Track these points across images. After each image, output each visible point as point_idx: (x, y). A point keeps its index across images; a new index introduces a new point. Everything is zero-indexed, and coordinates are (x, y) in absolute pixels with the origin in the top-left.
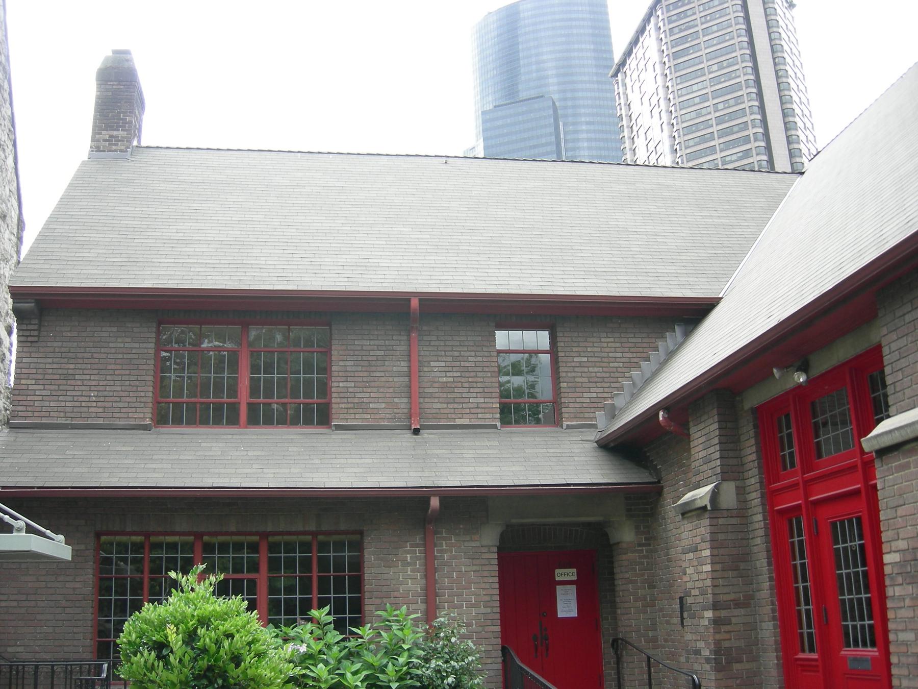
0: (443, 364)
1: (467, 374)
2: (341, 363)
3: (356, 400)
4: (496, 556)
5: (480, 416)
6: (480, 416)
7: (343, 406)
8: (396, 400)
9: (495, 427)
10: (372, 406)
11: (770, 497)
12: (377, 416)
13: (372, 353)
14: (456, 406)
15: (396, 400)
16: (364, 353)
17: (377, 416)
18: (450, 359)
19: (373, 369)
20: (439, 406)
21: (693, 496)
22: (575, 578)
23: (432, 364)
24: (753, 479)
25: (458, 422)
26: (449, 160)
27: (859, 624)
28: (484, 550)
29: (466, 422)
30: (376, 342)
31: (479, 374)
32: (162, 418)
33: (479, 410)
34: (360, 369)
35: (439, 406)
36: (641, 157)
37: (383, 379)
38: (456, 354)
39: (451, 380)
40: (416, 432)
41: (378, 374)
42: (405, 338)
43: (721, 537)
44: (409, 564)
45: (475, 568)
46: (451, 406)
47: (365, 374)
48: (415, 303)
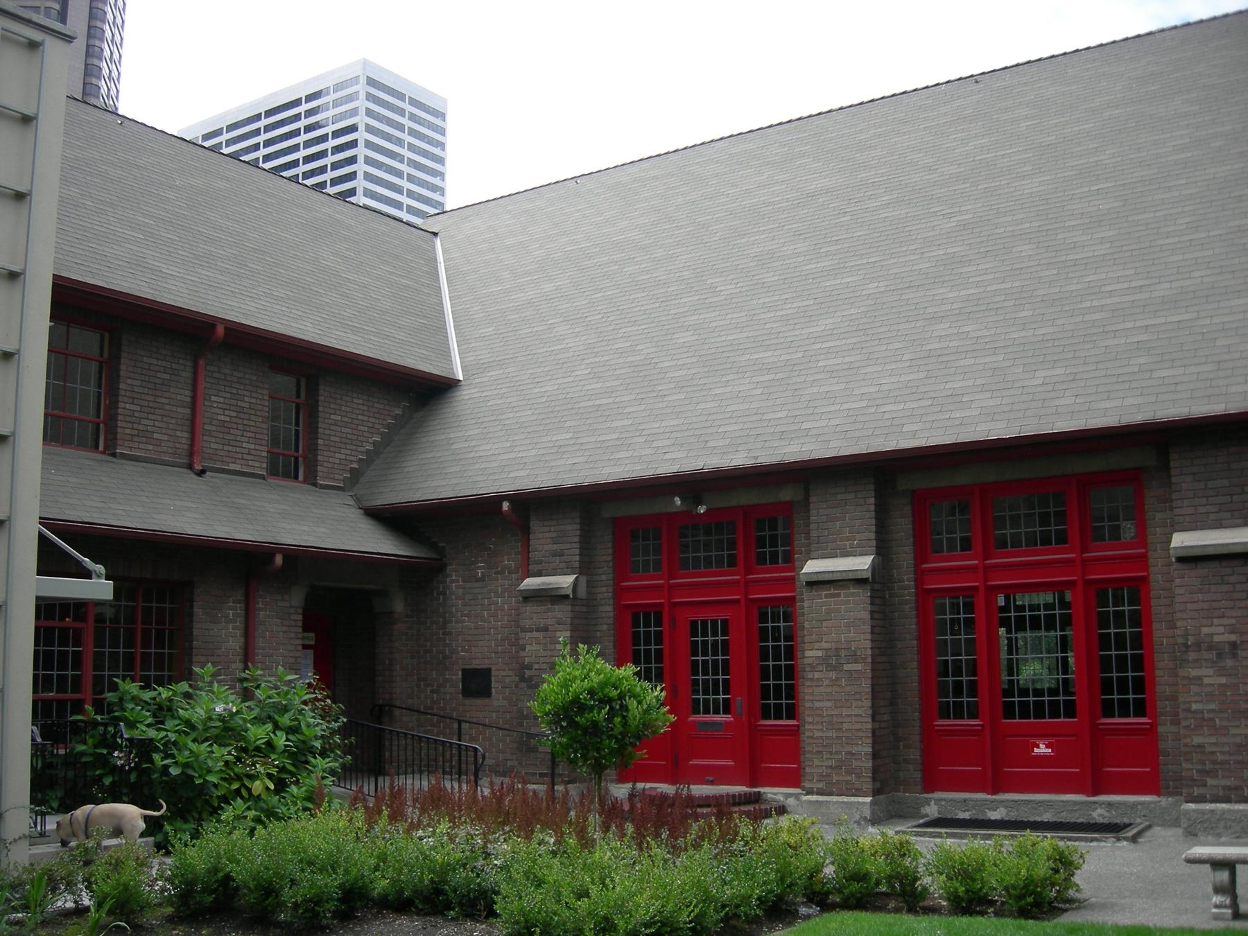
0: (222, 400)
1: (242, 415)
2: (129, 381)
3: (141, 427)
4: (300, 617)
5: (250, 463)
6: (250, 463)
7: (128, 431)
8: (178, 433)
9: (263, 477)
10: (156, 436)
11: (619, 593)
12: (159, 449)
13: (159, 375)
14: (231, 448)
15: (178, 433)
16: (152, 373)
17: (159, 449)
18: (228, 395)
19: (159, 393)
20: (216, 446)
21: (543, 584)
22: (312, 643)
23: (213, 398)
24: (605, 575)
25: (232, 467)
26: (126, 122)
27: (711, 697)
28: (292, 611)
29: (238, 468)
30: (164, 364)
31: (253, 418)
32: (274, 471)
33: (250, 457)
34: (146, 391)
35: (216, 446)
36: (100, 103)
37: (167, 407)
38: (234, 391)
39: (228, 419)
40: (201, 473)
41: (163, 400)
42: (189, 363)
43: (577, 621)
44: (231, 621)
45: (284, 629)
46: (226, 448)
47: (151, 398)
48: (220, 330)
